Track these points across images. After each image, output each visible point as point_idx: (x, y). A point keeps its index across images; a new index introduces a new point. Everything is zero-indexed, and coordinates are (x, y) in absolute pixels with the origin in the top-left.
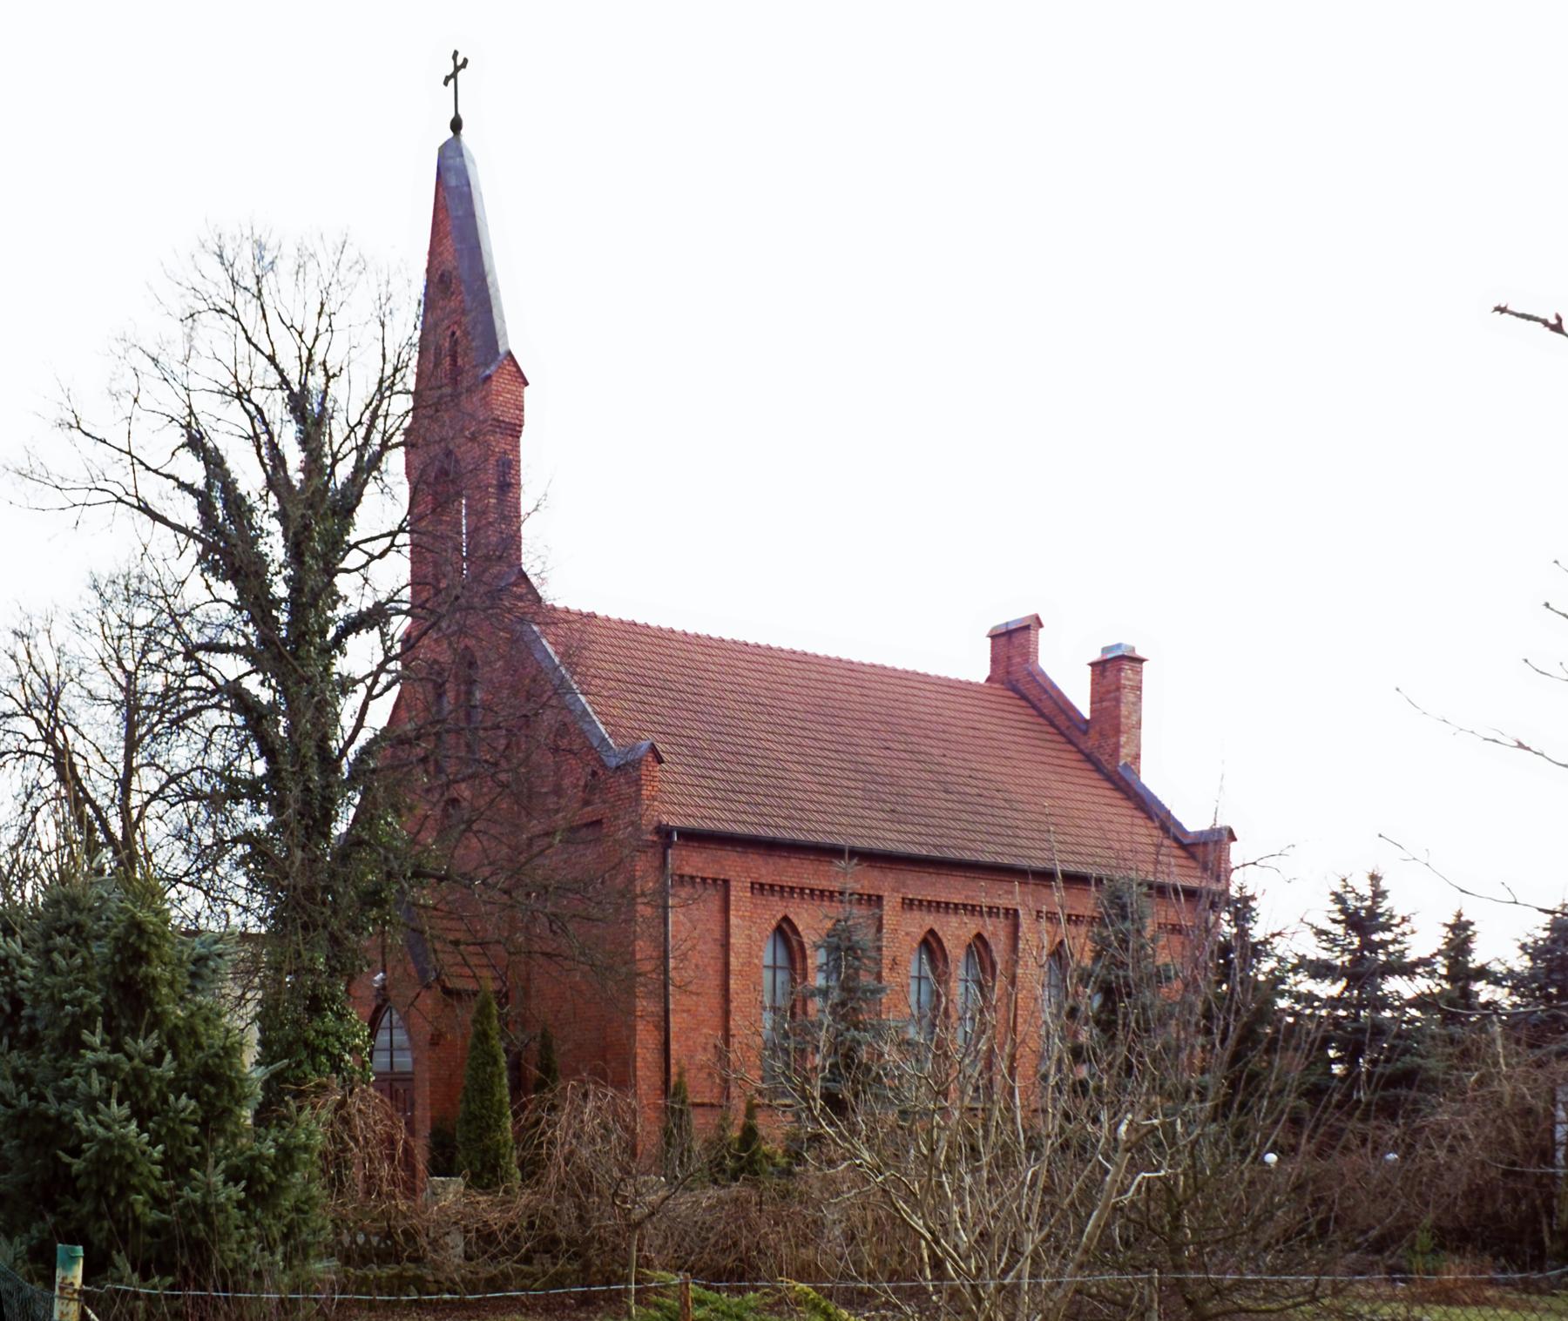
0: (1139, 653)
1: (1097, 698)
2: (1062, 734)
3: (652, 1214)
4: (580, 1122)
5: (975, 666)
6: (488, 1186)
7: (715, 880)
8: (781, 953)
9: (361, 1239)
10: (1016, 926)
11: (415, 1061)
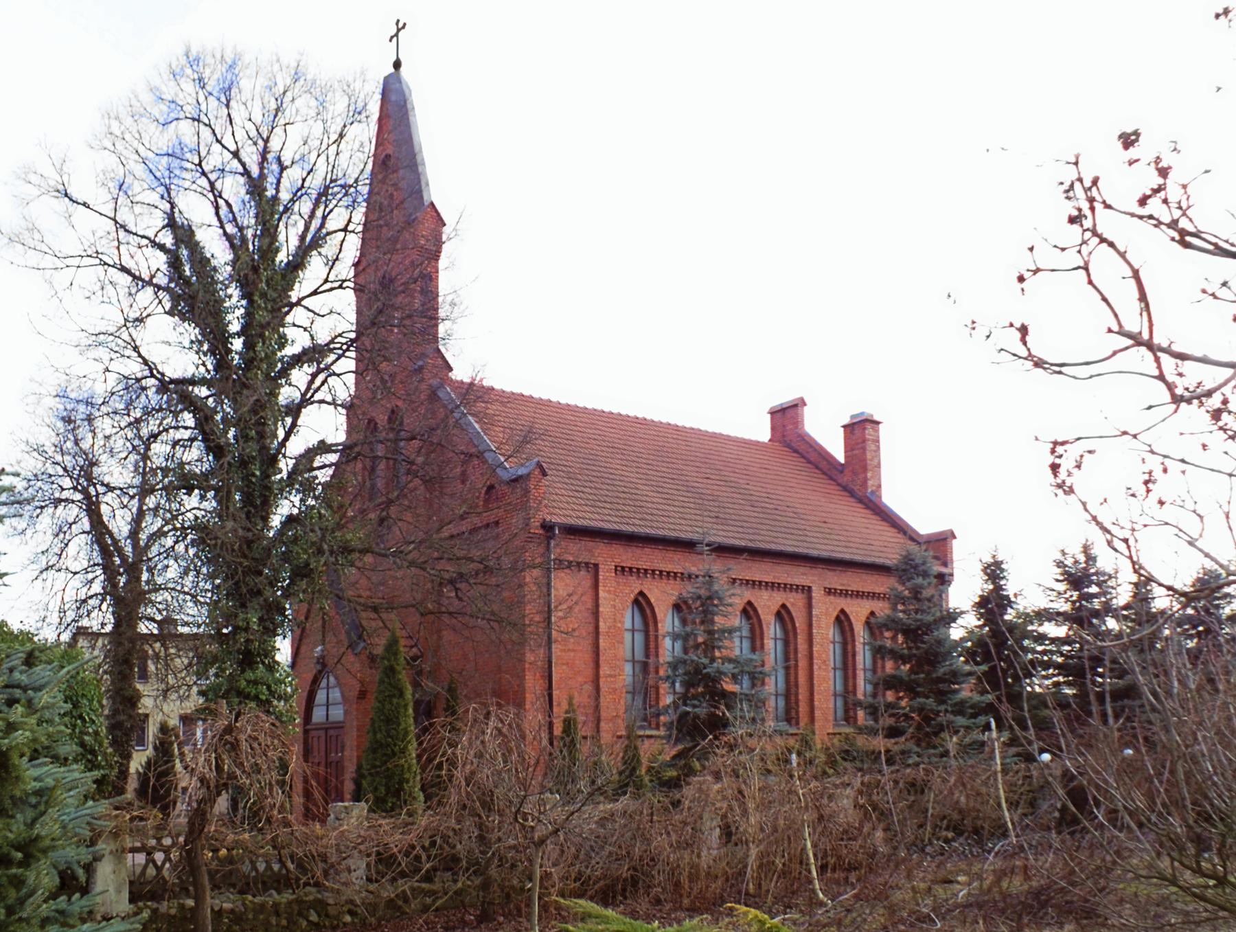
0: (876, 418)
1: (849, 448)
2: (824, 473)
3: (556, 831)
4: (478, 747)
5: (763, 433)
6: (392, 809)
7: (587, 564)
8: (638, 623)
9: (261, 867)
10: (810, 598)
11: (346, 713)
